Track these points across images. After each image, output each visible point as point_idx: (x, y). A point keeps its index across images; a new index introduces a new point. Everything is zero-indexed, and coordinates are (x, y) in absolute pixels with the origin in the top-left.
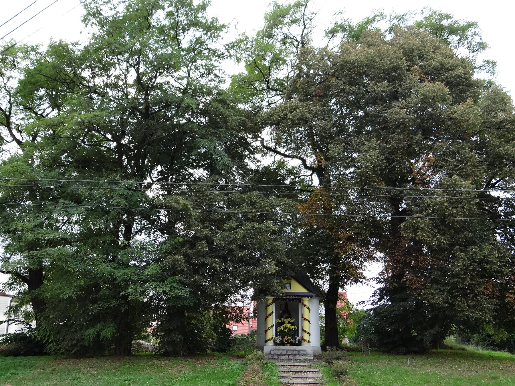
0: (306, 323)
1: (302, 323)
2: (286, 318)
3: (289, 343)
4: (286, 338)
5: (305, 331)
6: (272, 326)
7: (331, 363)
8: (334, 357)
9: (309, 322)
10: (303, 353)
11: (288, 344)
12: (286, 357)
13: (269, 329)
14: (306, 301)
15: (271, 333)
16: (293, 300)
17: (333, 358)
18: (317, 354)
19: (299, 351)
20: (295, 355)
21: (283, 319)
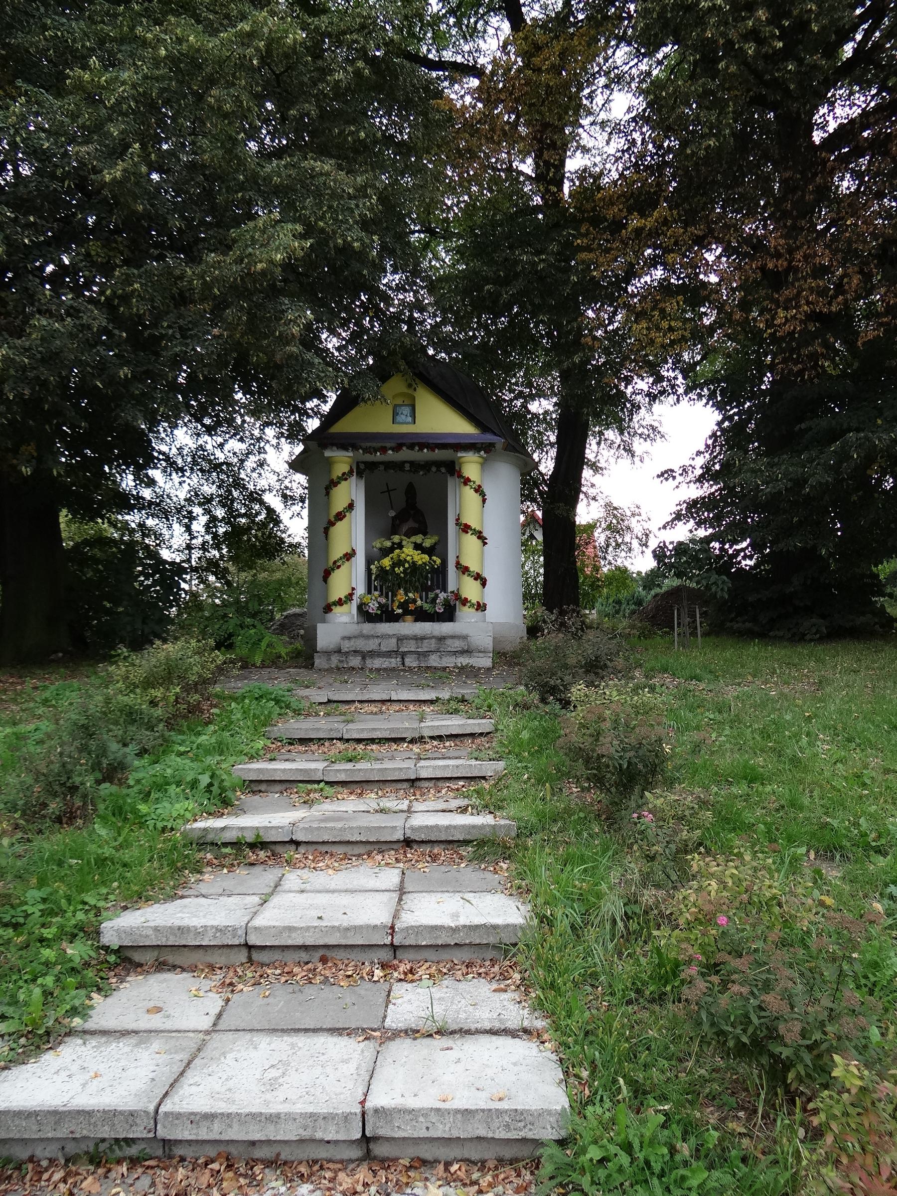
0: (471, 541)
2: (408, 535)
3: (410, 613)
4: (401, 596)
6: (349, 556)
7: (553, 690)
8: (572, 661)
10: (457, 645)
11: (409, 617)
12: (394, 662)
13: (336, 566)
14: (471, 466)
15: (351, 579)
16: (426, 466)
17: (566, 666)
18: (508, 648)
19: (441, 639)
20: (426, 654)
21: (396, 539)
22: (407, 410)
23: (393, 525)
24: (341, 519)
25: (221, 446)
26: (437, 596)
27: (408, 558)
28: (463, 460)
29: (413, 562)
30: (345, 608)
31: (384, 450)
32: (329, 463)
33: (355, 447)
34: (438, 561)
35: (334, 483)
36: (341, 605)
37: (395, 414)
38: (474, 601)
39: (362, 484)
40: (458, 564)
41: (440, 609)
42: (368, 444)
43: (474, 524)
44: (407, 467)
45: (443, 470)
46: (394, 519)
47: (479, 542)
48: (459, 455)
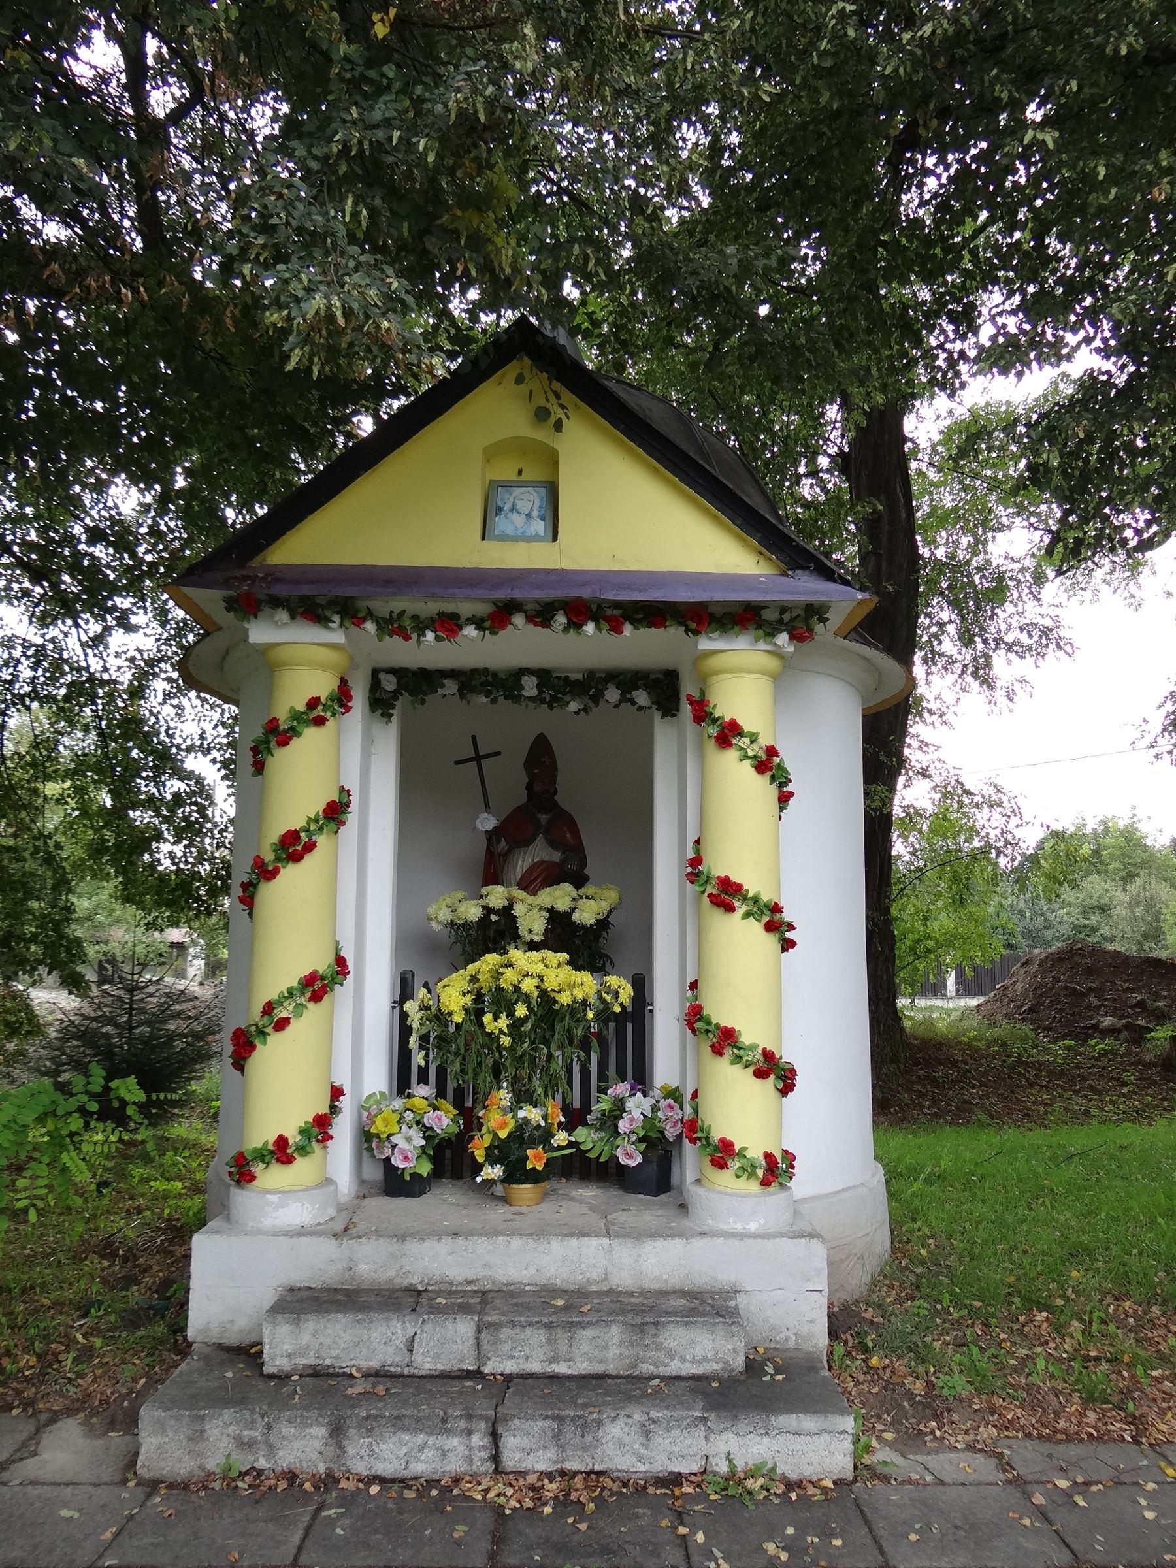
0: (739, 935)
1: (695, 943)
2: (531, 884)
4: (499, 1117)
5: (725, 1040)
9: (775, 923)
10: (700, 1349)
14: (742, 680)
16: (589, 686)
19: (645, 1310)
21: (497, 896)
22: (530, 500)
23: (490, 853)
24: (297, 858)
25: (98, 641)
26: (619, 1107)
27: (528, 986)
28: (714, 662)
29: (544, 994)
30: (302, 1170)
31: (448, 624)
32: (267, 665)
33: (350, 612)
34: (627, 993)
35: (281, 734)
36: (288, 1160)
37: (490, 511)
38: (755, 1153)
39: (388, 740)
40: (695, 1017)
41: (630, 1156)
42: (397, 605)
43: (753, 882)
44: (530, 687)
45: (642, 697)
46: (492, 836)
47: (771, 942)
48: (705, 644)
